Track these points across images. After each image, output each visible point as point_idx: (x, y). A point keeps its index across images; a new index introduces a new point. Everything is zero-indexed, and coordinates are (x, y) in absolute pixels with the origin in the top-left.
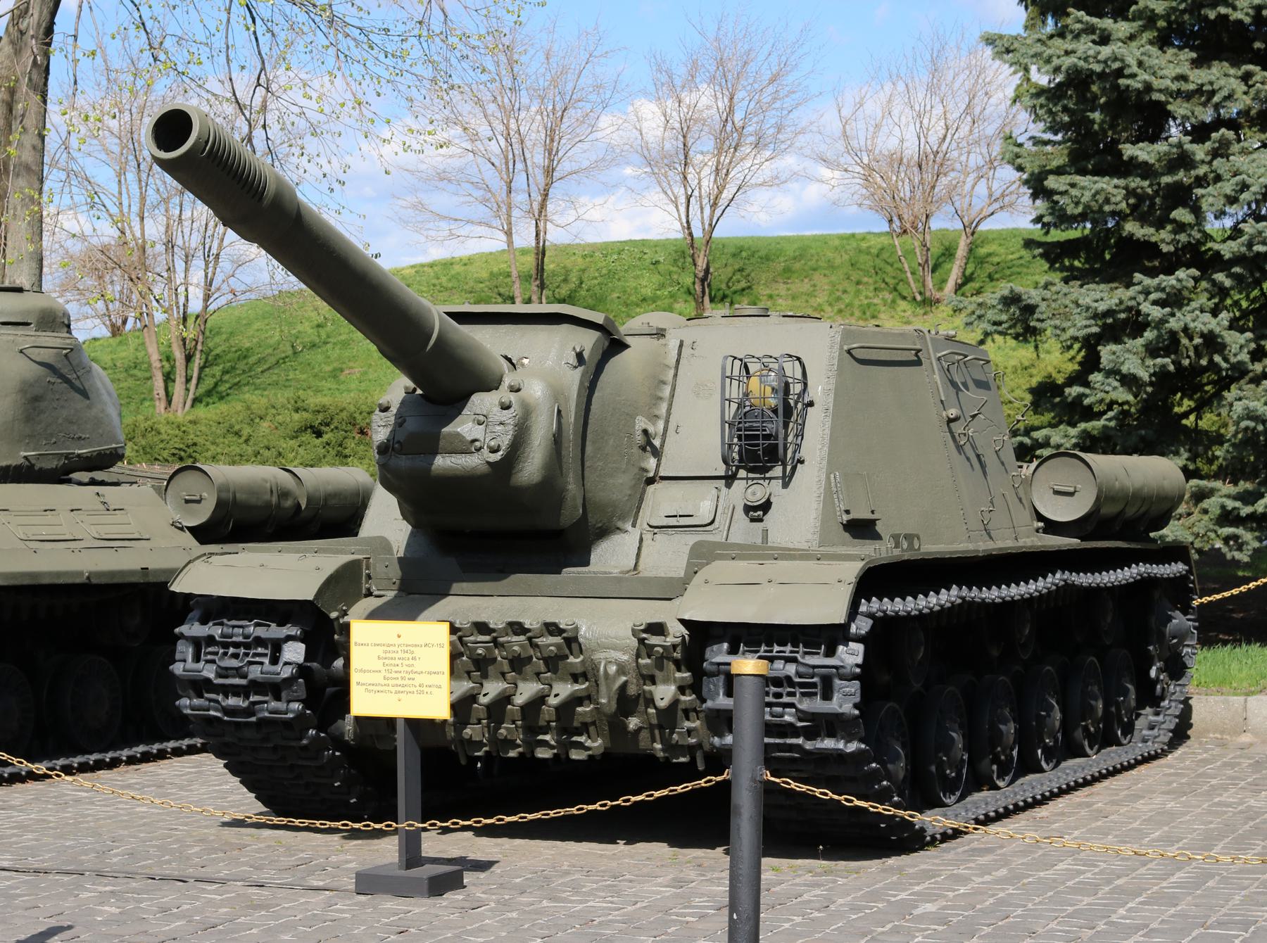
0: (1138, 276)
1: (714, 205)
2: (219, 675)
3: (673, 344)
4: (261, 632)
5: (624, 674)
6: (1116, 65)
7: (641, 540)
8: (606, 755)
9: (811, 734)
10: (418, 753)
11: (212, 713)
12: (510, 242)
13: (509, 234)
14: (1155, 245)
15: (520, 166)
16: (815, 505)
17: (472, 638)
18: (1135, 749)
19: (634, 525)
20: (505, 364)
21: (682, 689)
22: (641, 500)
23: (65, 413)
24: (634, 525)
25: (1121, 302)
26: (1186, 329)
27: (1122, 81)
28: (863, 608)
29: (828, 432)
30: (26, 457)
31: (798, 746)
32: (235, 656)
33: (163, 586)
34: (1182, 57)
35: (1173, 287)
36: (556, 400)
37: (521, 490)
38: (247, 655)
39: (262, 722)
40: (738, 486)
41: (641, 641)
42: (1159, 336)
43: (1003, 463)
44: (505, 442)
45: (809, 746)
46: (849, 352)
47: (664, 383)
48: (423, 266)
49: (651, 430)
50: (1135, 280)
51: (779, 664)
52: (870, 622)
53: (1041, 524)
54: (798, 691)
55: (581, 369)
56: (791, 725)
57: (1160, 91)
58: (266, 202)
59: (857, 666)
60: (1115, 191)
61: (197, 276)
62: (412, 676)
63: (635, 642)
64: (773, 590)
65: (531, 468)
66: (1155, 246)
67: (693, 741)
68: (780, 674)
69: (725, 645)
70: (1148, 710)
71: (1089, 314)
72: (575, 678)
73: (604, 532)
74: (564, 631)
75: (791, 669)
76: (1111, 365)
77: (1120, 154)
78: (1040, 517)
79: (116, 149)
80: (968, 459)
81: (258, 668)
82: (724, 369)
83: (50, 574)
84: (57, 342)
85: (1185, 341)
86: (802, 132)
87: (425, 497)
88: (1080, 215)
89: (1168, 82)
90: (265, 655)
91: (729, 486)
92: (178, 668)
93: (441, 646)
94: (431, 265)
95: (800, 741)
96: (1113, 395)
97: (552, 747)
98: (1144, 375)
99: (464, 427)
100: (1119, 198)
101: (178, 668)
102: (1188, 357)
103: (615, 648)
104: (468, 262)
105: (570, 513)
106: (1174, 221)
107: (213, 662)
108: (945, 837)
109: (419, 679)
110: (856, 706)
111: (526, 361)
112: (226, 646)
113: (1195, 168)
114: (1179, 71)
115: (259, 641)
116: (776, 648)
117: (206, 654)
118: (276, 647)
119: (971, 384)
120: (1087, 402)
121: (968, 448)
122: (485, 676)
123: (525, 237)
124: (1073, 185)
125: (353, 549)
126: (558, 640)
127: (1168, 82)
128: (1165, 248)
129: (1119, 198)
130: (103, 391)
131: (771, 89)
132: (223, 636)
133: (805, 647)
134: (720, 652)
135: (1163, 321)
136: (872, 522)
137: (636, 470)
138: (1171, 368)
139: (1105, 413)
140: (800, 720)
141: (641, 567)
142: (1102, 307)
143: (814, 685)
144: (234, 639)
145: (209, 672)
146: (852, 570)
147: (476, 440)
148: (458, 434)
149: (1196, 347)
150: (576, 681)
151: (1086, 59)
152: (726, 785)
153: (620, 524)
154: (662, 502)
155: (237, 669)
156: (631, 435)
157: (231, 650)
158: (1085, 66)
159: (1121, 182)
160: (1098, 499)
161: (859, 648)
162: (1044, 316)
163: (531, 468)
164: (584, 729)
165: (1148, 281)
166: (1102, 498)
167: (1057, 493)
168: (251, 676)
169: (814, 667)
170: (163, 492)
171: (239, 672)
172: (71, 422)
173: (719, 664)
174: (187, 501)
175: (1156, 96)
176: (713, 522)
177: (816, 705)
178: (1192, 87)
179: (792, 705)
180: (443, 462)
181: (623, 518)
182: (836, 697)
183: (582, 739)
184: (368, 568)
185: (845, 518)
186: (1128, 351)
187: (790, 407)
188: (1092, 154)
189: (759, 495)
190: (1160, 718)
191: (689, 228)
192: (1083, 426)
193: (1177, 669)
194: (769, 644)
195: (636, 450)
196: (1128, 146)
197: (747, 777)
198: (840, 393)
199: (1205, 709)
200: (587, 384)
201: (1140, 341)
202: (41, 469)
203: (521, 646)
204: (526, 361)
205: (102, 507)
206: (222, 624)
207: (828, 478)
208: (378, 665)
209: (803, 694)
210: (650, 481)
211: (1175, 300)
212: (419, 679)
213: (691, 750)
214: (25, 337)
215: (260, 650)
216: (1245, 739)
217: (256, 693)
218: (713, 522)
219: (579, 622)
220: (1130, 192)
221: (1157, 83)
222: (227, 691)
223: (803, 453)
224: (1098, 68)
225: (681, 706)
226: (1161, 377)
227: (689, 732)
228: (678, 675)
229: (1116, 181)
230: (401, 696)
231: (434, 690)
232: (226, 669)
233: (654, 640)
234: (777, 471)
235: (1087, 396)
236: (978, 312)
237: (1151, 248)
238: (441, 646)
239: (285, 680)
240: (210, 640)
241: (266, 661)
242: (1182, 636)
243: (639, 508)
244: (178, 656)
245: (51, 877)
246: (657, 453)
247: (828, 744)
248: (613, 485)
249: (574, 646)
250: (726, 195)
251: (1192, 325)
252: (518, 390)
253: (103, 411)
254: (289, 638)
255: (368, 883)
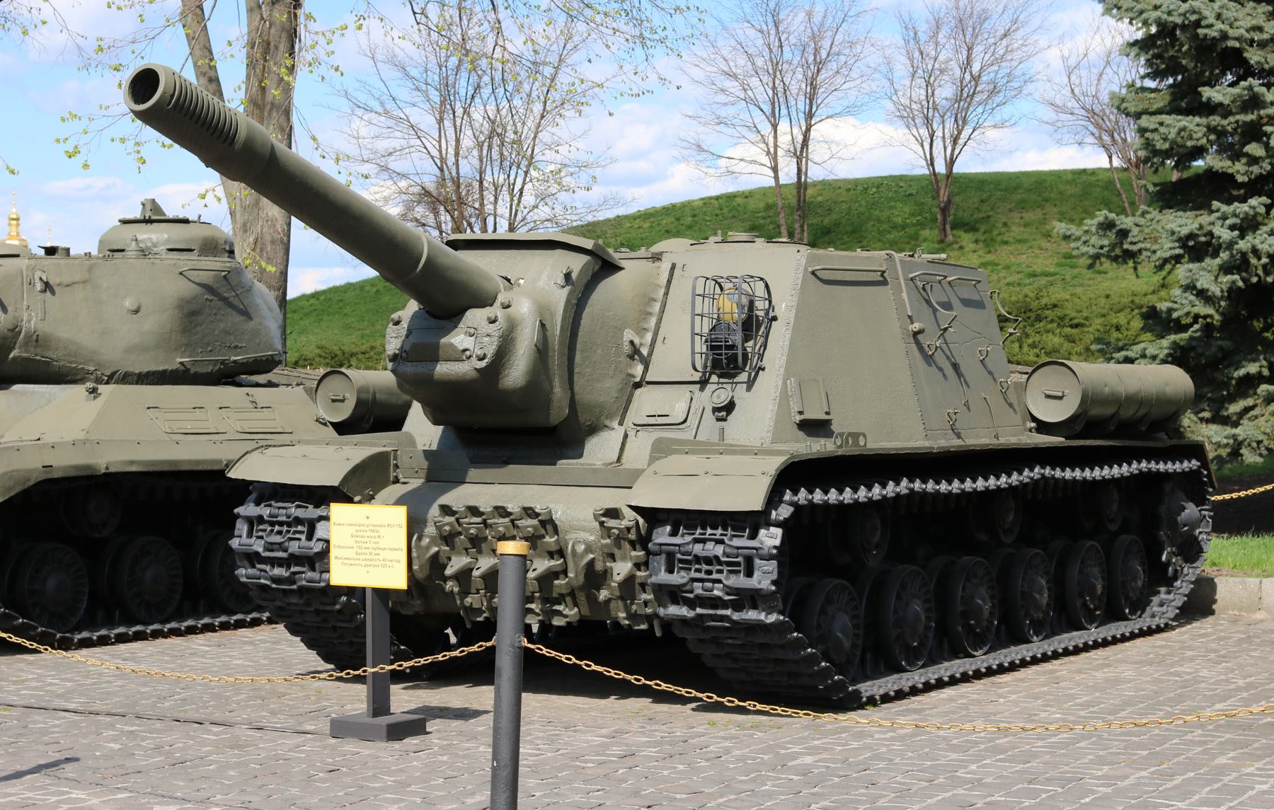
0: (1216, 204)
1: (955, 141)
2: (266, 549)
3: (665, 266)
4: (301, 513)
5: (592, 552)
6: (1193, 18)
7: (626, 436)
8: (583, 621)
9: (737, 606)
10: (388, 617)
11: (262, 581)
12: (776, 178)
13: (775, 169)
14: (1232, 176)
15: (784, 111)
16: (771, 407)
17: (466, 520)
18: (1145, 622)
19: (621, 424)
20: (501, 284)
21: (637, 566)
22: (629, 401)
23: (222, 326)
24: (621, 424)
25: (1201, 227)
26: (1255, 251)
27: (1200, 31)
28: (788, 496)
29: (787, 343)
30: (181, 363)
31: (727, 616)
32: (280, 533)
33: (221, 474)
34: (1260, 10)
35: (1247, 214)
36: (541, 314)
37: (508, 393)
38: (288, 532)
39: (301, 589)
40: (710, 388)
41: (602, 524)
42: (1232, 256)
43: (990, 373)
44: (490, 351)
45: (736, 616)
46: (813, 273)
47: (655, 300)
48: (710, 198)
49: (637, 341)
50: (1214, 208)
51: (710, 545)
52: (791, 509)
53: (1033, 425)
54: (725, 568)
55: (568, 288)
56: (719, 598)
57: (1236, 39)
58: (237, 146)
59: (775, 547)
60: (1196, 129)
61: (503, 209)
63: (597, 524)
64: (708, 480)
65: (516, 373)
66: (1232, 176)
67: (649, 611)
68: (710, 554)
69: (668, 528)
70: (1163, 589)
71: (1175, 237)
72: (551, 555)
73: (593, 429)
74: (537, 515)
75: (719, 550)
76: (1188, 281)
77: (1200, 94)
78: (1034, 419)
79: (437, 100)
80: (940, 369)
81: (296, 544)
82: (694, 288)
83: (190, 462)
84: (218, 266)
85: (1253, 261)
86: (1031, 80)
87: (449, 403)
88: (1167, 151)
89: (1243, 31)
90: (302, 532)
91: (702, 389)
92: (234, 543)
93: (400, 526)
94: (717, 198)
95: (728, 612)
96: (1195, 310)
97: (538, 615)
98: (1216, 290)
99: (458, 339)
100: (1200, 135)
101: (234, 543)
102: (1257, 275)
103: (584, 530)
104: (747, 195)
105: (559, 410)
106: (1247, 155)
107: (261, 537)
109: (383, 555)
110: (774, 583)
111: (521, 282)
112: (272, 524)
113: (1264, 108)
114: (1254, 22)
115: (298, 521)
116: (709, 531)
117: (258, 531)
119: (956, 303)
120: (1175, 315)
121: (939, 357)
122: (480, 552)
123: (788, 174)
124: (1161, 124)
125: (385, 442)
126: (535, 522)
127: (1243, 31)
128: (1240, 179)
129: (1200, 135)
130: (264, 307)
131: (1004, 42)
132: (271, 516)
133: (733, 530)
134: (663, 534)
135: (1230, 245)
136: (828, 422)
137: (623, 376)
138: (1241, 284)
139: (1191, 325)
140: (728, 594)
141: (624, 459)
142: (1185, 231)
143: (738, 564)
144: (279, 519)
145: (258, 547)
146: (773, 464)
148: (452, 345)
149: (1264, 267)
150: (552, 558)
151: (1169, 13)
152: (493, 648)
153: (607, 422)
154: (646, 403)
155: (280, 544)
156: (618, 346)
157: (277, 528)
158: (1171, 19)
159: (1204, 121)
160: (1083, 401)
161: (778, 532)
162: (1136, 240)
163: (516, 373)
164: (560, 599)
165: (1224, 208)
166: (1088, 400)
167: (1048, 396)
168: (290, 550)
169: (738, 548)
170: (313, 393)
171: (281, 547)
172: (228, 333)
173: (661, 545)
174: (334, 401)
175: (1231, 43)
176: (685, 421)
177: (740, 581)
178: (1266, 36)
179: (719, 581)
180: (444, 369)
181: (610, 417)
182: (756, 574)
183: (560, 608)
184: (395, 459)
185: (798, 418)
186: (1204, 269)
187: (753, 324)
188: (1186, 100)
189: (723, 397)
190: (1171, 596)
191: (932, 164)
192: (1173, 337)
193: (1192, 551)
194: (704, 528)
195: (623, 359)
196: (1207, 88)
197: (507, 643)
198: (801, 310)
199: (1227, 590)
200: (574, 301)
201: (1218, 261)
202: (196, 373)
203: (506, 527)
204: (521, 282)
205: (250, 405)
206: (270, 506)
207: (785, 383)
208: (351, 542)
209: (730, 572)
210: (638, 385)
211: (1247, 226)
212: (383, 555)
213: (649, 619)
214: (185, 262)
215: (300, 528)
216: (1259, 616)
217: (296, 565)
218: (685, 421)
219: (551, 506)
220: (1211, 129)
221: (1231, 33)
222: (274, 562)
223: (765, 363)
224: (1179, 20)
225: (638, 581)
226: (1232, 292)
227: (646, 603)
228: (634, 553)
229: (1197, 119)
230: (370, 569)
231: (395, 564)
232: (272, 544)
233: (611, 523)
234: (743, 377)
235: (1176, 310)
236: (1083, 239)
237: (1228, 179)
238: (400, 526)
239: (317, 554)
240: (260, 519)
241: (303, 537)
242: (1195, 524)
243: (626, 410)
244: (236, 533)
245: (99, 717)
246: (646, 363)
247: (752, 615)
248: (597, 386)
249: (549, 527)
250: (965, 135)
251: (1260, 247)
252: (509, 306)
253: (260, 324)
255: (341, 729)
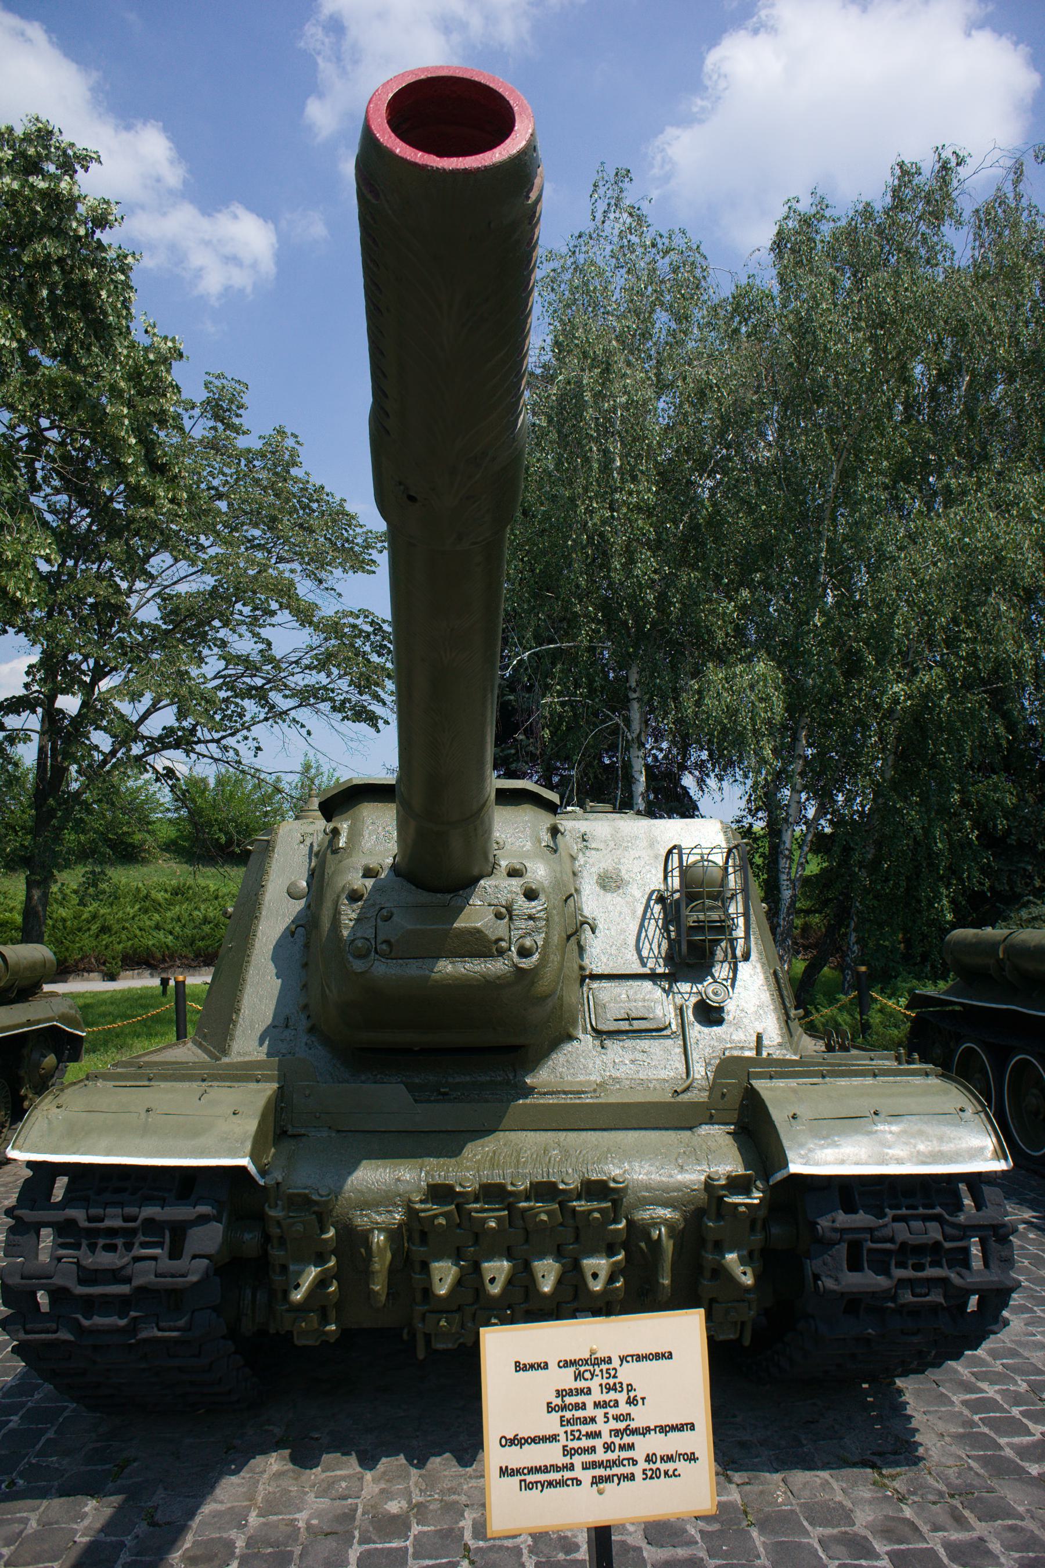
62: (627, 1440)
108: (294, 1136)
118: (178, 1232)
147: (501, 940)
171: (116, 1276)
208: (551, 1424)
212: (644, 1446)
231: (681, 1466)
254: (203, 1219)
